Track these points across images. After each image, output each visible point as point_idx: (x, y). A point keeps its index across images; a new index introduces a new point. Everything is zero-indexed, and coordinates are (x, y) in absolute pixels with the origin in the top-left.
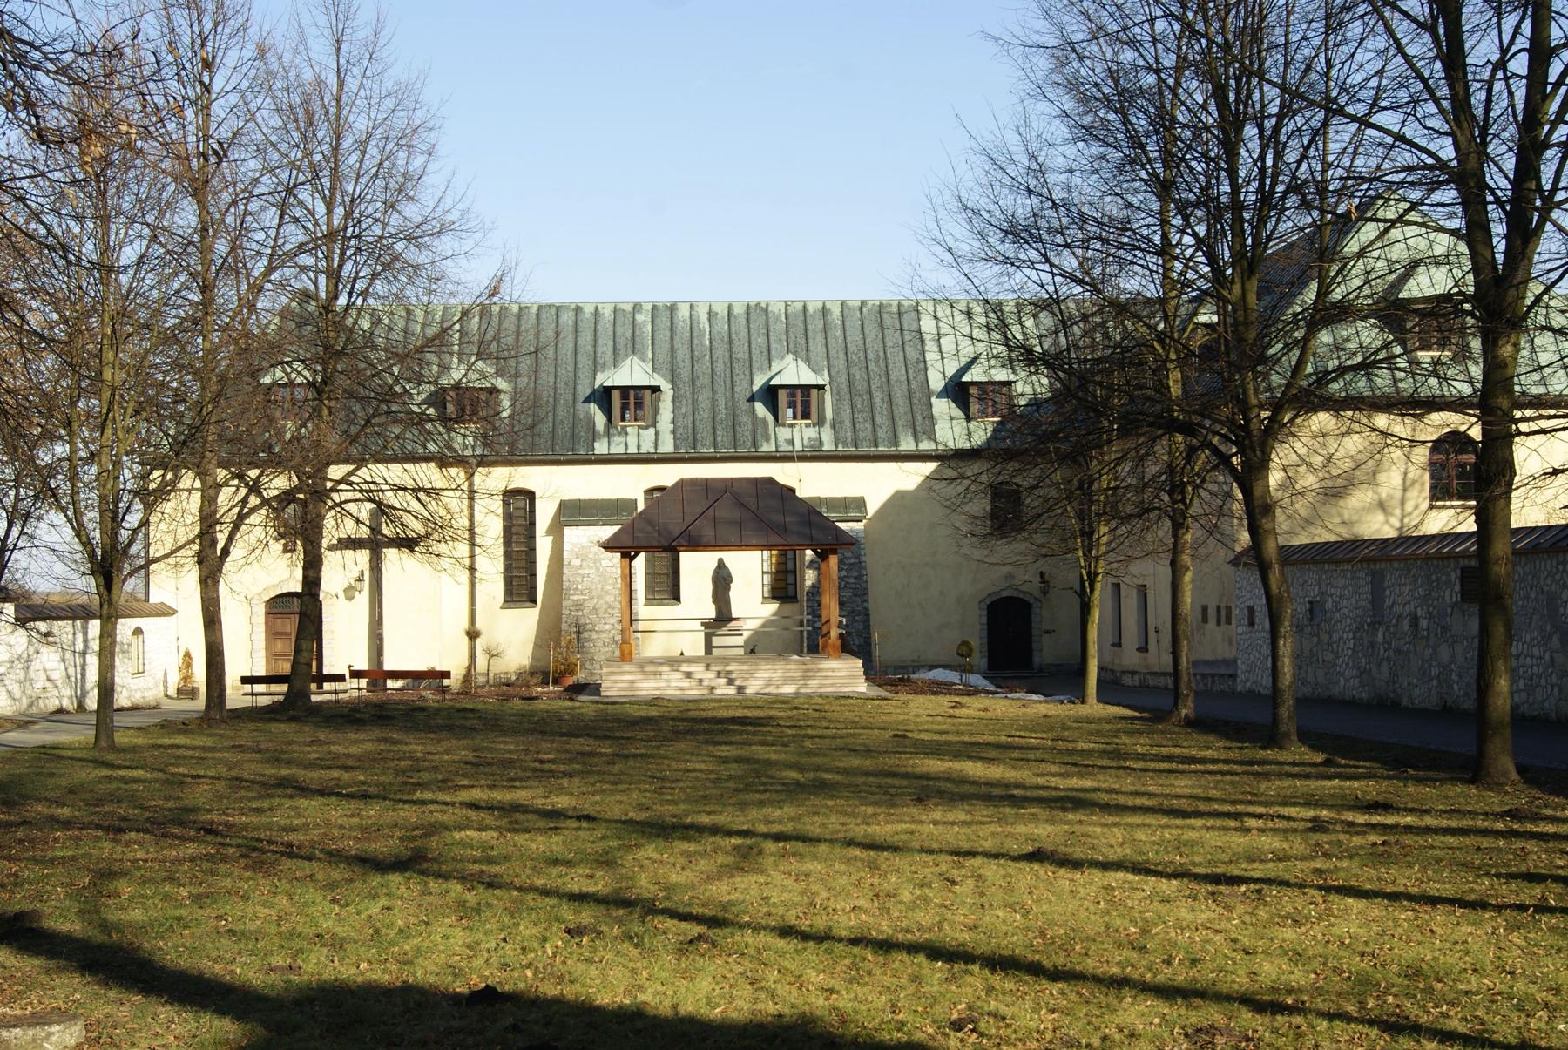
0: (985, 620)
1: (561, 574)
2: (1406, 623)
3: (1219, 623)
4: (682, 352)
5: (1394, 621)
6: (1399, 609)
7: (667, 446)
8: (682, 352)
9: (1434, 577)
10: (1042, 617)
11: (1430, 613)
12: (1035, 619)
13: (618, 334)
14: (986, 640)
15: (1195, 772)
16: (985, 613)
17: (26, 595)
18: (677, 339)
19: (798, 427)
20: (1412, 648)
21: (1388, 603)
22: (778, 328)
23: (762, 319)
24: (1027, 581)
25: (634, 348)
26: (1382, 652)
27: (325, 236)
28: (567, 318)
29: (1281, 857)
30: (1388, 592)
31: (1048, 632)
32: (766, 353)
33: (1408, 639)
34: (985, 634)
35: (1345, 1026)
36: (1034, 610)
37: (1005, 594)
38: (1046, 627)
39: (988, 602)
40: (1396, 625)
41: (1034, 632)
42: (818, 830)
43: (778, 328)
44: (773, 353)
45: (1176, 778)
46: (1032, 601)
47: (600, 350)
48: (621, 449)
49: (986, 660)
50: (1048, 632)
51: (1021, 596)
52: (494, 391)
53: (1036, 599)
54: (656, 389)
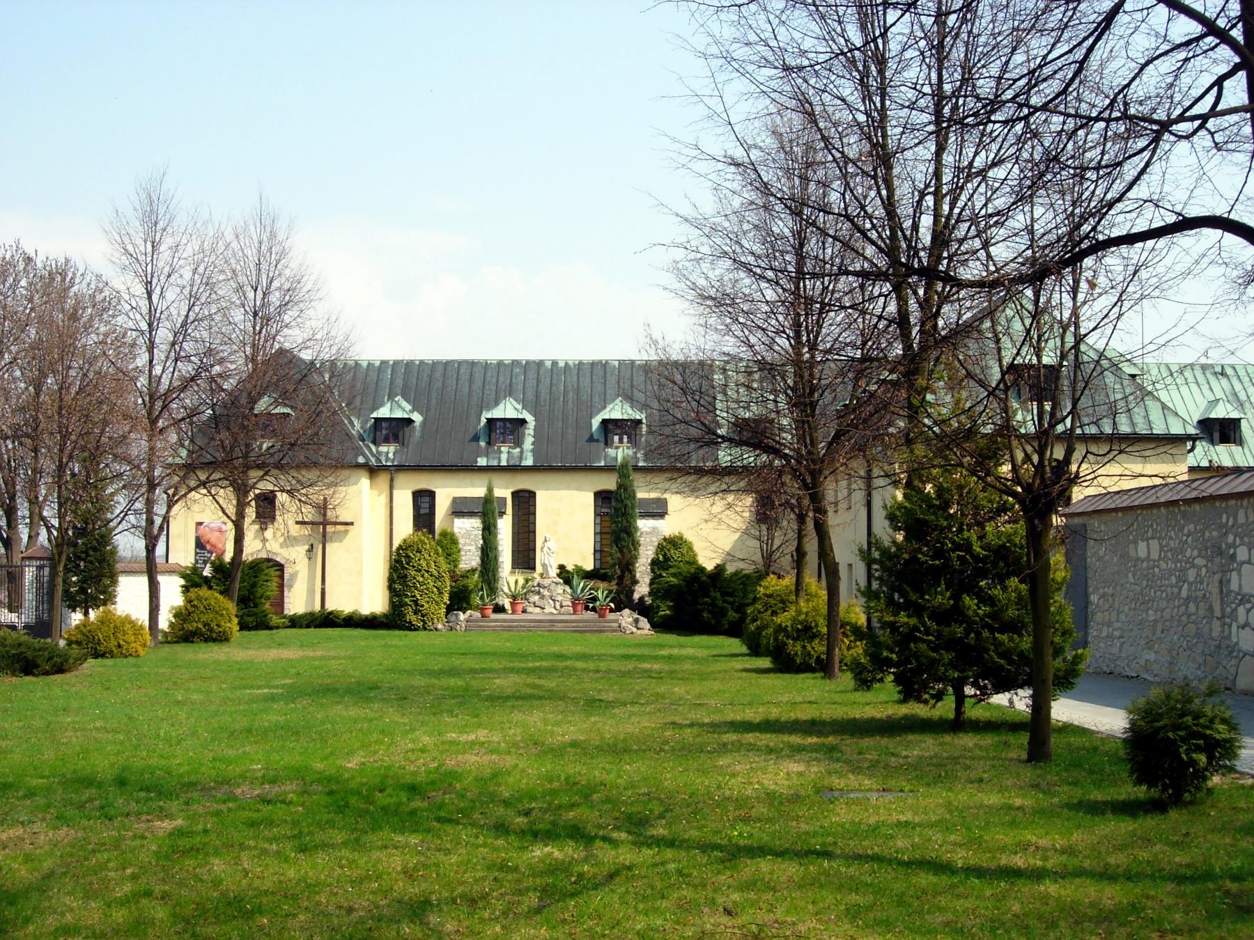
1: (829, 594)
4: (544, 394)
7: (529, 461)
8: (544, 394)
13: (500, 382)
15: (541, 658)
17: (1193, 711)
18: (541, 386)
19: (621, 449)
22: (612, 380)
23: (601, 373)
25: (510, 392)
27: (897, 289)
28: (438, 373)
32: (603, 396)
35: (77, 673)
42: (773, 787)
43: (612, 380)
44: (608, 396)
47: (487, 392)
48: (495, 463)
52: (410, 421)
54: (523, 422)
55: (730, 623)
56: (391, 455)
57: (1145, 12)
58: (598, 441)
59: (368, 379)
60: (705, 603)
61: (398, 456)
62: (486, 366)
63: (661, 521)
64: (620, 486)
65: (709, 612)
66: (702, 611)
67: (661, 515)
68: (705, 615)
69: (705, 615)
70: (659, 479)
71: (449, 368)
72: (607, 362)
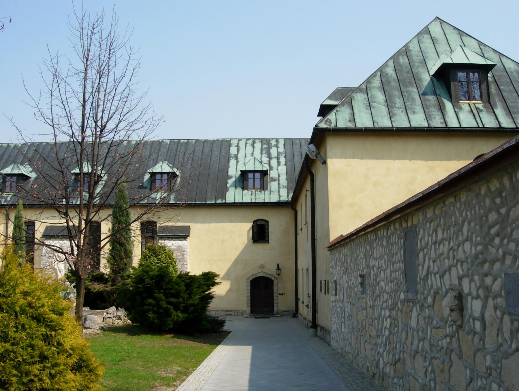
0: (249, 288)
2: (448, 301)
3: (325, 294)
5: (430, 300)
6: (435, 281)
9: (493, 217)
10: (277, 288)
11: (487, 289)
12: (275, 288)
14: (250, 298)
16: (249, 284)
20: (455, 345)
21: (422, 273)
24: (270, 270)
26: (416, 342)
29: (381, 234)
30: (421, 255)
31: (281, 294)
33: (448, 330)
34: (249, 295)
36: (274, 283)
37: (259, 275)
38: (280, 291)
39: (251, 279)
40: (432, 306)
41: (275, 294)
43: (163, 150)
45: (500, 101)
46: (273, 279)
49: (250, 308)
50: (281, 294)
51: (268, 276)
52: (28, 178)
53: (275, 278)
55: (175, 323)
56: (9, 199)
57: (80, 21)
58: (146, 188)
59: (12, 153)
60: (150, 304)
61: (13, 199)
62: (187, 143)
63: (184, 242)
64: (514, 242)
65: (155, 312)
66: (147, 311)
67: (185, 237)
68: (151, 315)
69: (151, 315)
70: (183, 212)
71: (214, 145)
72: (162, 141)
